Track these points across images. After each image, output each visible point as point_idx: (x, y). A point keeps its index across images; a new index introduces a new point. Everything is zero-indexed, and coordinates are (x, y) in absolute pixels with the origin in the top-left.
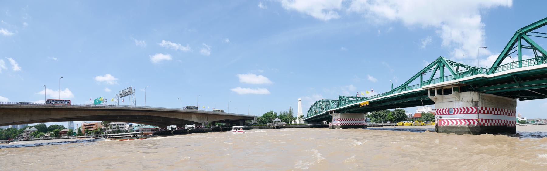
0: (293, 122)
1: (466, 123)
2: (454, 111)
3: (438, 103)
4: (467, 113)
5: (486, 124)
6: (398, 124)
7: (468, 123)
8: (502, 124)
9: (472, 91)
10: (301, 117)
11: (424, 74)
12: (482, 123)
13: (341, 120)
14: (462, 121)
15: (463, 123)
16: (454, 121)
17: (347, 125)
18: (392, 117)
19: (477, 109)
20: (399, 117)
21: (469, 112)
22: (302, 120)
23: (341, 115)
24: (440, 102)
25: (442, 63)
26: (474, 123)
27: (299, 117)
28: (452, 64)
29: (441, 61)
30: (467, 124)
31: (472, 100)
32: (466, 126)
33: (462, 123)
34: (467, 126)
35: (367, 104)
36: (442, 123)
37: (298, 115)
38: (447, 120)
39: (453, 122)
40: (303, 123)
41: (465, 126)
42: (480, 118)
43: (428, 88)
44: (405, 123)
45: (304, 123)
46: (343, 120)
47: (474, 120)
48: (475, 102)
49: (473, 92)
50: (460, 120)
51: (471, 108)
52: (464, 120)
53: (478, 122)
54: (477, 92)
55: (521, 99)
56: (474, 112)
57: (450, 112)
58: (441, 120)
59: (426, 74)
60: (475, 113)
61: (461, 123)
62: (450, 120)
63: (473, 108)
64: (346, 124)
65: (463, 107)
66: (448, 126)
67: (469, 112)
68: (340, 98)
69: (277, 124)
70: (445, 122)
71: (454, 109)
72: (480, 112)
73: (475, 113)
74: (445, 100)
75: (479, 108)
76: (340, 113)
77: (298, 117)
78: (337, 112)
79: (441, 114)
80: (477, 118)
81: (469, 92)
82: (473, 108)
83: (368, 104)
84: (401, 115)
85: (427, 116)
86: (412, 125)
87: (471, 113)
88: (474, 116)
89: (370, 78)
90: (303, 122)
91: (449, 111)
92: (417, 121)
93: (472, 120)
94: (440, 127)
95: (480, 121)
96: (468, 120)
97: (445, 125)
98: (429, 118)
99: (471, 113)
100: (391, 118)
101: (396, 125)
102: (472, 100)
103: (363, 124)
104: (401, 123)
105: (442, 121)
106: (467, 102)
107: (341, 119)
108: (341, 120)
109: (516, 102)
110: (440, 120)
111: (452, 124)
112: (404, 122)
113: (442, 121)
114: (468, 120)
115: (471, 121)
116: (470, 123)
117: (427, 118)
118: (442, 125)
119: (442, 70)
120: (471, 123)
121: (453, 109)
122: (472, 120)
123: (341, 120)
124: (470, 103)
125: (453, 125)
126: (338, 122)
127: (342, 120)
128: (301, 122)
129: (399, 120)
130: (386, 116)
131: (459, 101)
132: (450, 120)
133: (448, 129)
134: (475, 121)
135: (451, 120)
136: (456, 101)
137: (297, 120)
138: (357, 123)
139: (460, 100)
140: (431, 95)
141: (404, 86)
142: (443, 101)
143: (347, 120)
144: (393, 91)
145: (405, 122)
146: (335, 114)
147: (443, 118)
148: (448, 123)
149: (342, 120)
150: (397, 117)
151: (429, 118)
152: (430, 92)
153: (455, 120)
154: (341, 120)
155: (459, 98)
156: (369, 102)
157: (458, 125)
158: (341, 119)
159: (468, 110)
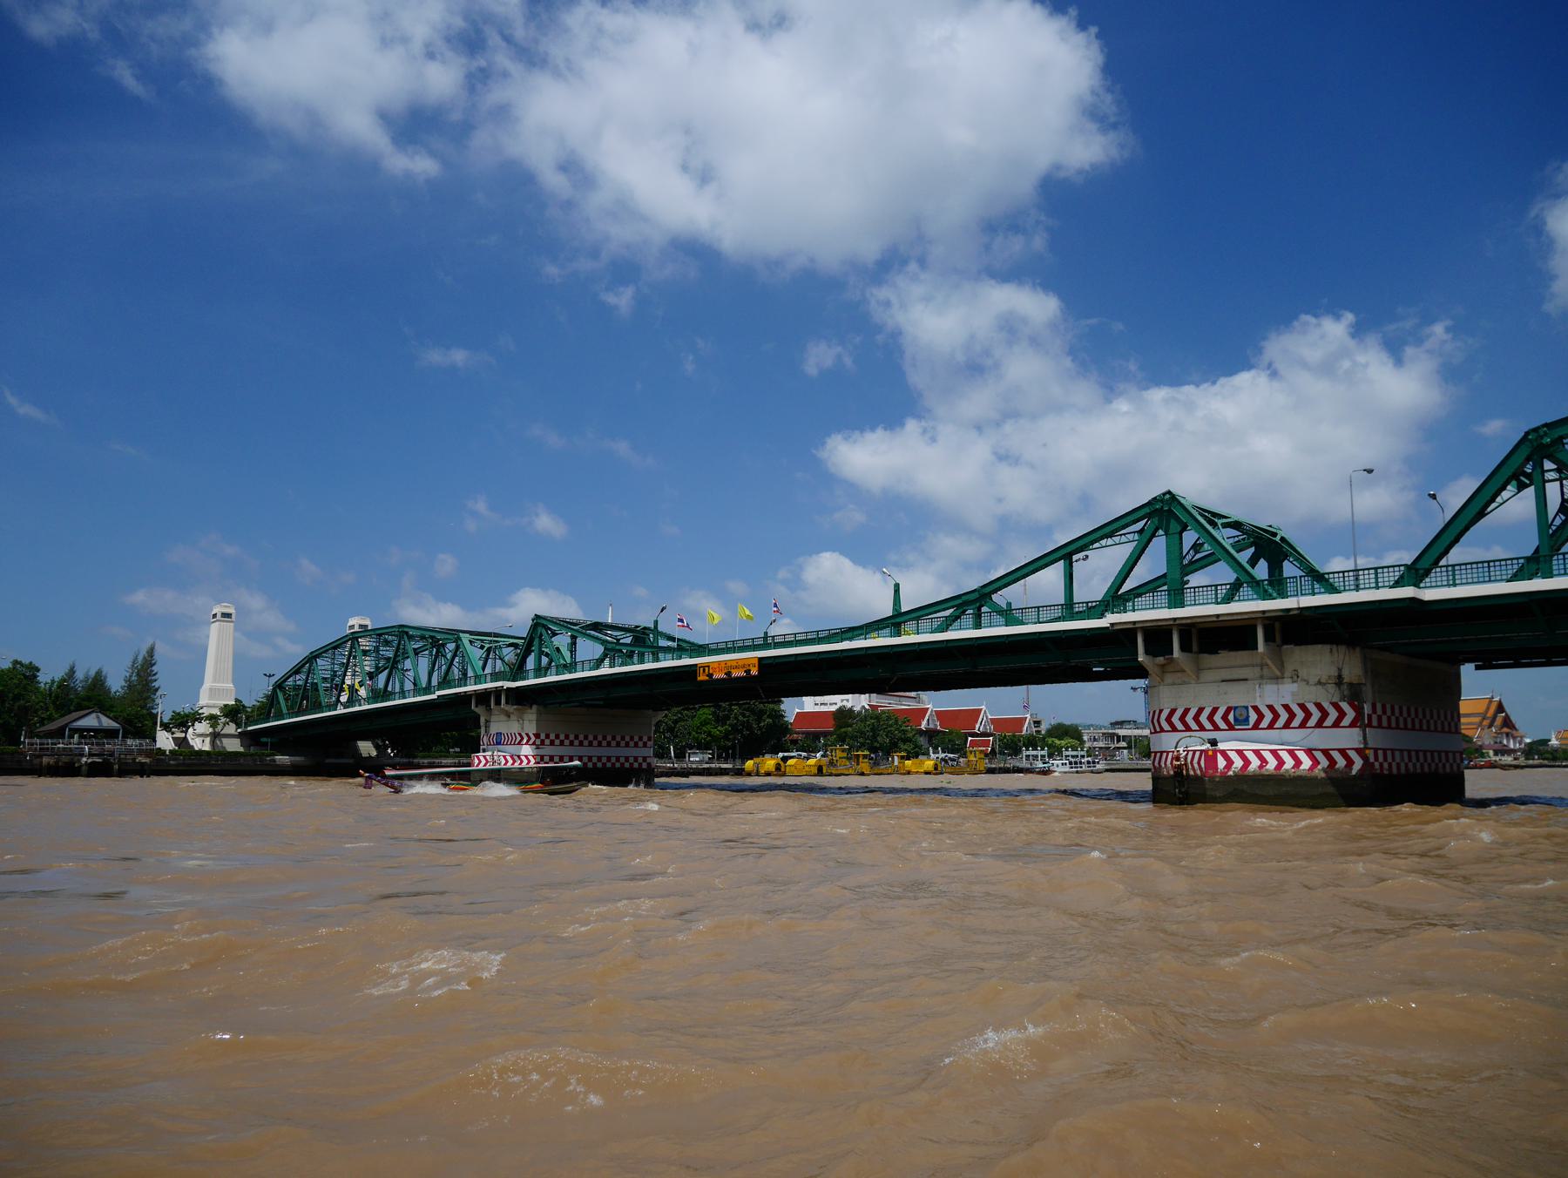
0: (165, 741)
1: (1316, 762)
2: (1253, 717)
3: (1174, 684)
4: (1319, 724)
5: (1386, 765)
6: (749, 764)
7: (1324, 763)
8: (590, 765)
9: (1337, 644)
10: (226, 716)
11: (1081, 555)
12: (1377, 765)
13: (543, 742)
14: (1302, 755)
15: (1307, 763)
16: (1268, 756)
17: (636, 765)
18: (716, 732)
19: (1359, 711)
20: (749, 727)
21: (1265, 723)
22: (231, 729)
23: (539, 713)
24: (1184, 683)
25: (1177, 519)
26: (1350, 762)
27: (216, 712)
28: (1214, 524)
29: (1170, 511)
30: (1319, 767)
31: (1340, 677)
32: (1319, 772)
33: (1301, 763)
34: (1323, 775)
35: (748, 672)
36: (1221, 763)
37: (203, 701)
38: (1240, 753)
39: (1264, 761)
40: (233, 745)
41: (1313, 774)
42: (1370, 746)
43: (1137, 626)
44: (790, 762)
45: (242, 749)
46: (552, 743)
47: (1349, 752)
48: (1351, 685)
49: (1343, 649)
50: (1292, 753)
51: (1336, 706)
52: (1309, 752)
53: (1365, 758)
54: (1358, 650)
55: (1486, 662)
56: (1346, 721)
57: (1236, 719)
58: (1215, 752)
59: (1087, 556)
60: (1353, 725)
61: (1298, 762)
62: (1288, 751)
63: (1345, 706)
64: (613, 764)
65: (1300, 702)
66: (1246, 773)
67: (1329, 722)
68: (540, 630)
69: (96, 749)
70: (1230, 762)
71: (1256, 709)
72: (1370, 725)
73: (1353, 725)
74: (1207, 675)
75: (1367, 709)
76: (535, 707)
77: (206, 712)
78: (522, 698)
79: (1217, 728)
80: (1362, 746)
81: (1327, 647)
82: (1345, 706)
83: (754, 672)
84: (759, 720)
85: (873, 729)
86: (820, 769)
87: (1336, 724)
88: (1348, 738)
89: (546, 523)
90: (237, 741)
91: (1231, 717)
92: (839, 754)
93: (1343, 752)
94: (1212, 778)
95: (1370, 754)
96: (1326, 752)
97: (1231, 773)
98: (883, 739)
99: (1336, 724)
100: (709, 734)
101: (740, 772)
102: (1340, 677)
103: (644, 766)
104: (770, 762)
105: (1219, 756)
106: (1319, 683)
107: (543, 736)
108: (543, 742)
109: (1457, 677)
110: (1210, 753)
111: (1261, 767)
112: (781, 755)
113: (1219, 756)
114: (1326, 752)
115: (1336, 755)
116: (1332, 762)
117: (875, 737)
118: (1221, 773)
119: (1146, 540)
120: (1233, 763)
121: (1251, 709)
122: (1343, 752)
123: (538, 742)
124: (1332, 688)
125: (1264, 771)
126: (527, 750)
127: (547, 742)
128: (226, 741)
129: (754, 748)
130: (676, 722)
131: (1276, 679)
132: (1288, 751)
133: (1245, 787)
134: (1352, 754)
135: (1257, 753)
136: (1262, 677)
137: (203, 727)
138: (618, 759)
139: (1283, 674)
140: (1147, 652)
141: (975, 602)
142: (1198, 677)
143: (572, 744)
144: (895, 622)
145: (785, 759)
146: (511, 708)
147: (1221, 746)
148: (1247, 762)
149: (547, 742)
150: (741, 732)
151: (883, 739)
152: (1145, 641)
153: (1274, 753)
154: (539, 741)
155: (1282, 667)
156: (760, 659)
157: (1287, 770)
158: (543, 736)
159: (522, 739)
